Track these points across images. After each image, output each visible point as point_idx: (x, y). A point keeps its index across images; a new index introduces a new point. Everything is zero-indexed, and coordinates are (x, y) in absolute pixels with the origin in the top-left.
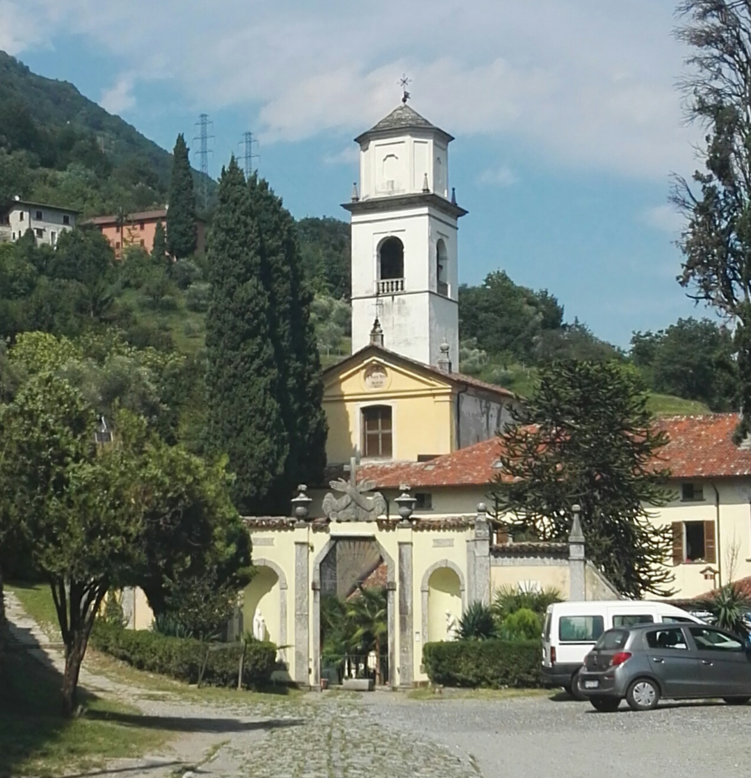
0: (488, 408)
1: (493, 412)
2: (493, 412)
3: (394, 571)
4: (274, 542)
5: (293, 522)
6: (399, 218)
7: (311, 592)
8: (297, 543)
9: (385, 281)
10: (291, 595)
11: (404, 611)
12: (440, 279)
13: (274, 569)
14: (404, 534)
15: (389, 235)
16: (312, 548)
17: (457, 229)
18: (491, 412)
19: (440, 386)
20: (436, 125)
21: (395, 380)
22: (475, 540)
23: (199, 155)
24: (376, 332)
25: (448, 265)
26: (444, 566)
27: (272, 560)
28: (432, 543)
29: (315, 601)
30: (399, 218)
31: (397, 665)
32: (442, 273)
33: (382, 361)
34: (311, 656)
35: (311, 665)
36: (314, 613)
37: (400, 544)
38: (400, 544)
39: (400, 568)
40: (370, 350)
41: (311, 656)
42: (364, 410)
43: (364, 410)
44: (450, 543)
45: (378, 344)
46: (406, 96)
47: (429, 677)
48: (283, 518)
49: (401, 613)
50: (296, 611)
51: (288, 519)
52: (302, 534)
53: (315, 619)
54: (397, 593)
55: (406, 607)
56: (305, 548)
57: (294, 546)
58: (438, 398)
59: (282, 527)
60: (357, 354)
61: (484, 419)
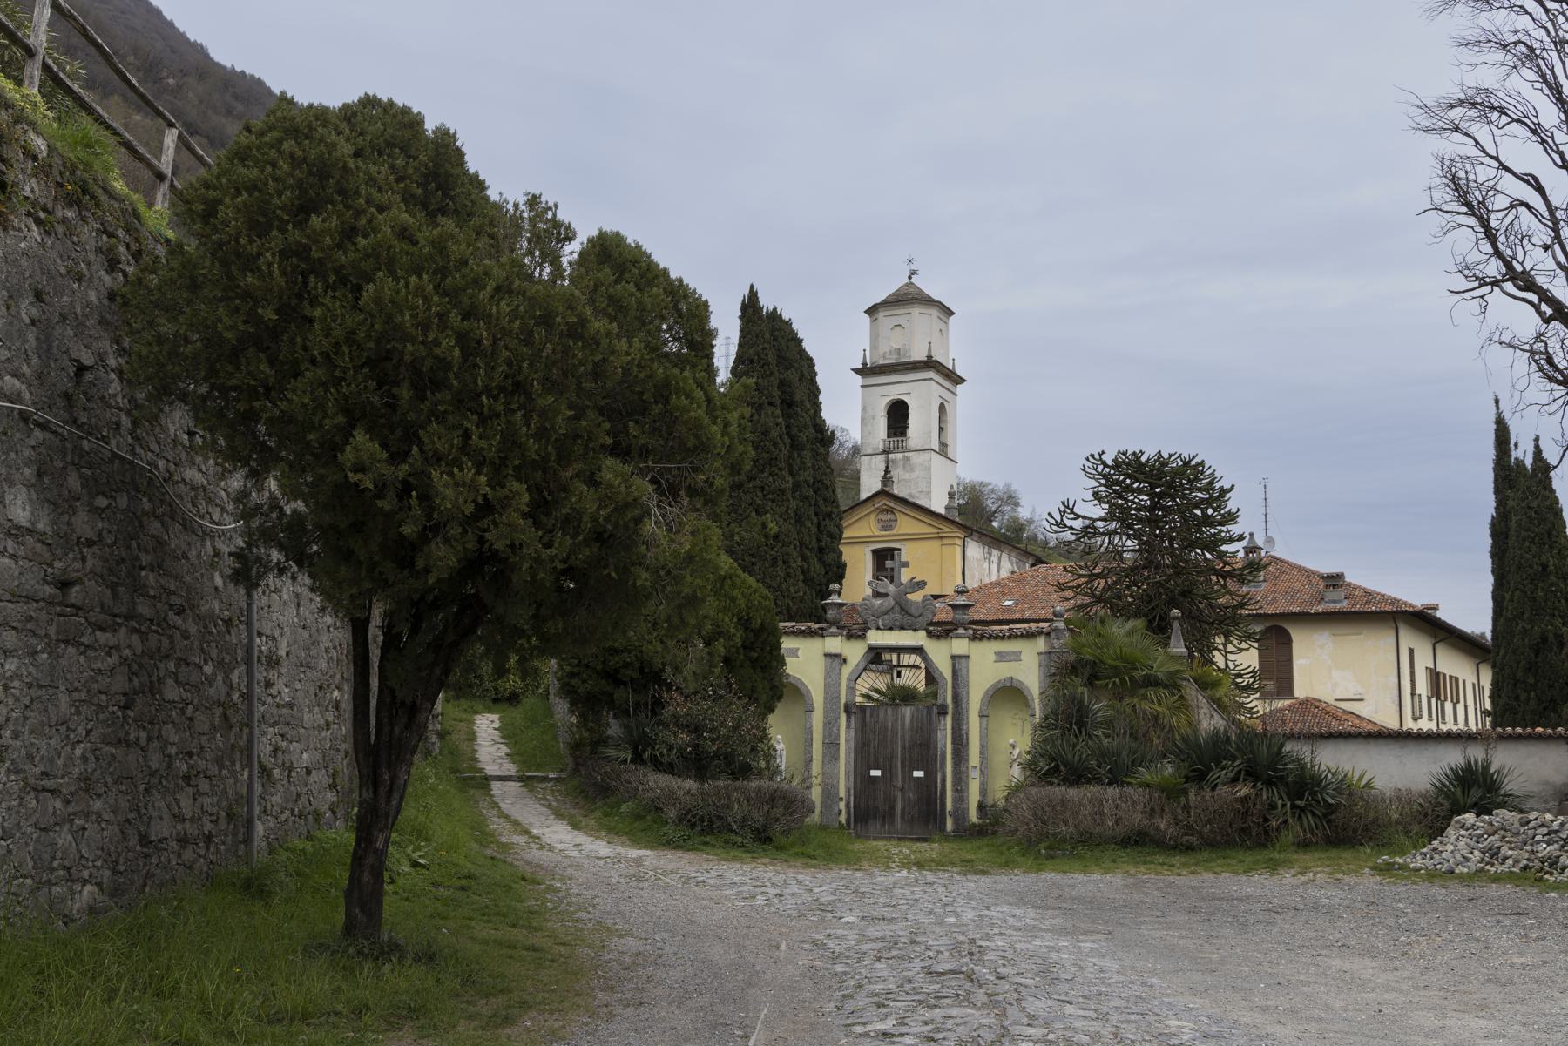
0: (990, 554)
1: (995, 558)
2: (995, 558)
3: (946, 691)
4: (800, 653)
5: (822, 629)
6: (906, 382)
7: (843, 717)
8: (826, 655)
9: (891, 439)
10: (817, 719)
11: (960, 741)
12: (942, 439)
13: (799, 686)
14: (960, 646)
15: (896, 397)
16: (845, 661)
17: (956, 395)
18: (992, 558)
19: (948, 530)
20: (936, 299)
21: (906, 524)
22: (1049, 653)
23: (723, 359)
24: (887, 479)
25: (949, 428)
26: (1009, 685)
27: (798, 676)
28: (993, 657)
29: (848, 727)
30: (906, 382)
31: (949, 806)
32: (943, 434)
33: (892, 505)
34: (842, 793)
35: (842, 805)
36: (847, 741)
37: (953, 657)
38: (953, 657)
39: (953, 687)
40: (882, 493)
41: (842, 793)
42: (875, 552)
43: (875, 552)
44: (1016, 656)
45: (886, 489)
46: (913, 273)
47: (490, 711)
48: (809, 624)
49: (953, 742)
50: (824, 738)
51: (817, 626)
52: (834, 644)
53: (848, 749)
54: (949, 719)
55: (961, 735)
56: (837, 662)
57: (823, 658)
58: (945, 542)
59: (809, 633)
60: (869, 499)
61: (986, 565)
